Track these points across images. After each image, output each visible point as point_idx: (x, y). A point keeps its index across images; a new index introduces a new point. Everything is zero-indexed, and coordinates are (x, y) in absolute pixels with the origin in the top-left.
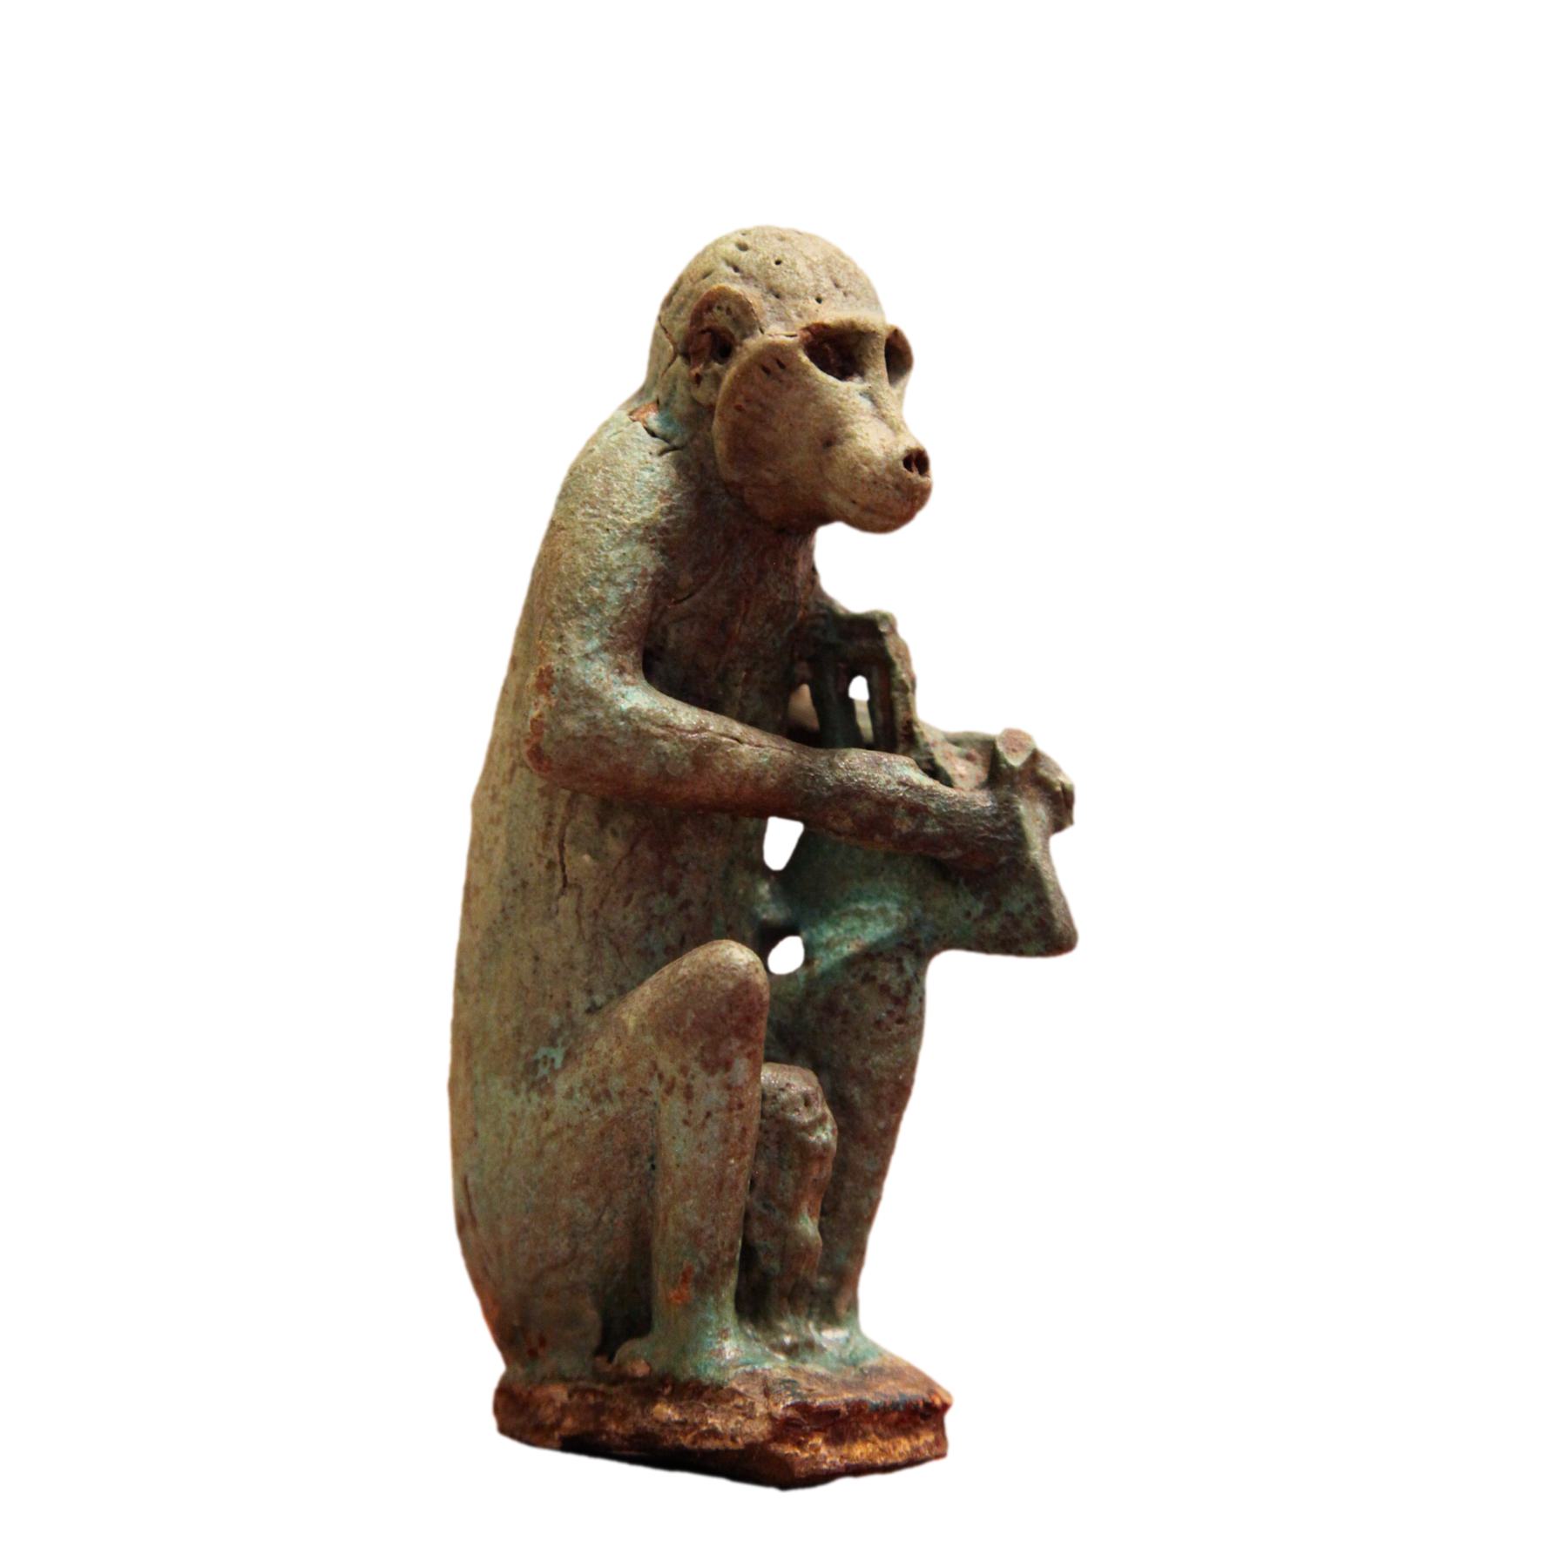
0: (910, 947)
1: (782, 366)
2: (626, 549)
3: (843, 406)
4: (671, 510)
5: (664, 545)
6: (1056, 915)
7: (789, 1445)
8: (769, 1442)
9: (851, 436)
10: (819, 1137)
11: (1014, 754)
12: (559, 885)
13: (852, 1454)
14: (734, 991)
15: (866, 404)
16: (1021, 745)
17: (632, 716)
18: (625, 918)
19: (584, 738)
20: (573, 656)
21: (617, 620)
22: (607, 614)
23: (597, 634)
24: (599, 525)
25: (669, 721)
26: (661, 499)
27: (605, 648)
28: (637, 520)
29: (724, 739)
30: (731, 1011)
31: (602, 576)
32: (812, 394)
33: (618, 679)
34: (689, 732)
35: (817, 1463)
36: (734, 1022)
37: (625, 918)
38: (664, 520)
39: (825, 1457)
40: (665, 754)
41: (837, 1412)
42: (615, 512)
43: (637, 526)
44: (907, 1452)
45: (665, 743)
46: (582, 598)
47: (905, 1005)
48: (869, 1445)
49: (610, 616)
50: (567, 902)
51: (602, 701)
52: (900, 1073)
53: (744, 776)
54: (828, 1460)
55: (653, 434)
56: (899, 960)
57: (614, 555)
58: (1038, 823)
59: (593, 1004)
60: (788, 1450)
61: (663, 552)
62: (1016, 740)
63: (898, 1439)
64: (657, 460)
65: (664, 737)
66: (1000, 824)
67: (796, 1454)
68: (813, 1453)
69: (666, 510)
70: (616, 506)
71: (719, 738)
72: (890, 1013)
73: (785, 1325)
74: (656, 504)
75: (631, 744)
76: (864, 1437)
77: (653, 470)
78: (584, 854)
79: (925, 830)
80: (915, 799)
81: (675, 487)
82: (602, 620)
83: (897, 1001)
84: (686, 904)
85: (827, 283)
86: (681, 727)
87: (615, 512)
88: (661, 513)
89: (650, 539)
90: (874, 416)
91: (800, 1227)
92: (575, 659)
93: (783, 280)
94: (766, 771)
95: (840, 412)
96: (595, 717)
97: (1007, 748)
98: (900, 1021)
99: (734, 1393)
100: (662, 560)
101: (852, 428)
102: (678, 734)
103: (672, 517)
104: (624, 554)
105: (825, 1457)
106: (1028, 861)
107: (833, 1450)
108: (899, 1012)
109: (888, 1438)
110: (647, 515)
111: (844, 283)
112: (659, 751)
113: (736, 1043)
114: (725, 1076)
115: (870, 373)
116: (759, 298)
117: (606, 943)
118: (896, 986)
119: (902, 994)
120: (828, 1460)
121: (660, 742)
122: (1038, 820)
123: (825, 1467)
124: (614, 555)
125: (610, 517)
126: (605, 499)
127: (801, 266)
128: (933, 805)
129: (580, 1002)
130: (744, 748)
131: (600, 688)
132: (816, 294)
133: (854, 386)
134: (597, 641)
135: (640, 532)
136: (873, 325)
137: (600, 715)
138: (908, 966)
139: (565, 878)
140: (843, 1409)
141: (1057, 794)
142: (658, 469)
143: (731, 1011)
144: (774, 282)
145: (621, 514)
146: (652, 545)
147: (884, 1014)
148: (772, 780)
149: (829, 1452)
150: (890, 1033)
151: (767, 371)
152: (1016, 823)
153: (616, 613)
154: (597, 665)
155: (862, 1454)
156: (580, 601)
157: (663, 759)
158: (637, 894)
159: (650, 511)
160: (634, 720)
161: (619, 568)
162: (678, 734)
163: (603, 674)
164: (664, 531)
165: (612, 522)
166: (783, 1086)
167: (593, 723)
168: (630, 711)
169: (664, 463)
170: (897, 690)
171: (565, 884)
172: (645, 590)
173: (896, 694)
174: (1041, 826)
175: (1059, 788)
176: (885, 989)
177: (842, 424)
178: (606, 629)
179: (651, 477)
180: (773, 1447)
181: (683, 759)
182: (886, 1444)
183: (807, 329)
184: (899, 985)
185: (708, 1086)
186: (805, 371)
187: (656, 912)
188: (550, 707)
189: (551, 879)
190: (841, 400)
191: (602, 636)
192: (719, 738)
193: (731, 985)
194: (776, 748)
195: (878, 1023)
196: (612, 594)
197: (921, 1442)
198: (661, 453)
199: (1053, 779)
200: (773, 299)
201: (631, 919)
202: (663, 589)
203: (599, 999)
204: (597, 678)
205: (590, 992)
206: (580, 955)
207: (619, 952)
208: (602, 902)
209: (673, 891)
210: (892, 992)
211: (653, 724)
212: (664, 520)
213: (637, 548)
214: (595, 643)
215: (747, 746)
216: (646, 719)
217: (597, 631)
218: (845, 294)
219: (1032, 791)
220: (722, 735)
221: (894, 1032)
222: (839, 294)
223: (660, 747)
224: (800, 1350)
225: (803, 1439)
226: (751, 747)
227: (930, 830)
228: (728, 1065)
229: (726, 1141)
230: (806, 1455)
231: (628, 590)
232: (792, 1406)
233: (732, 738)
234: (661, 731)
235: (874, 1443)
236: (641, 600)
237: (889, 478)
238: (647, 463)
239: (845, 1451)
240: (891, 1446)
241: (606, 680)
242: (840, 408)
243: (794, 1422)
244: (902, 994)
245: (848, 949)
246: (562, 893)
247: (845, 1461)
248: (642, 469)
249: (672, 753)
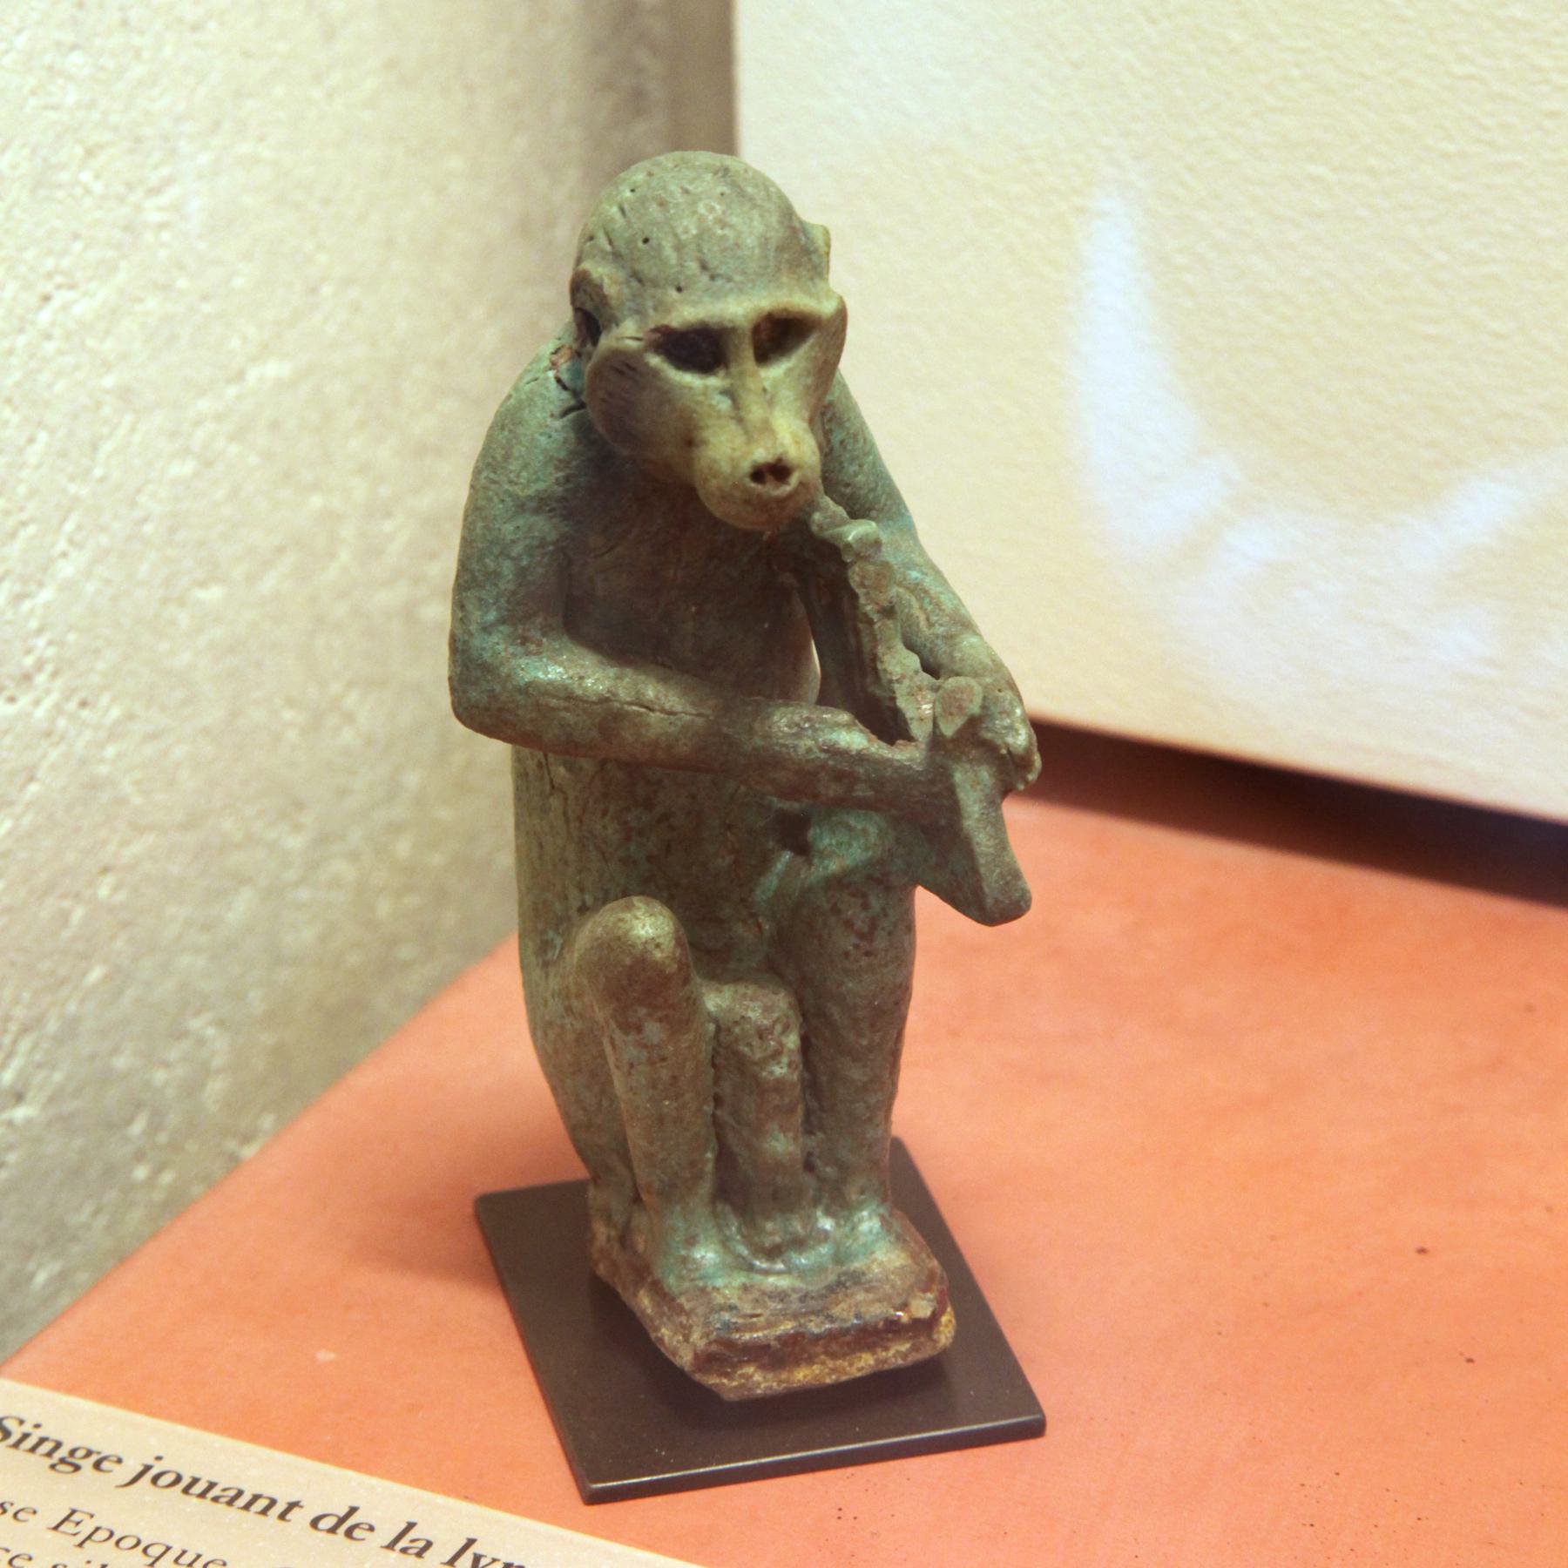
0: (879, 882)
1: (633, 369)
2: (521, 522)
3: (698, 409)
4: (567, 479)
5: (565, 512)
6: (987, 890)
7: (715, 1375)
8: (694, 1372)
9: (705, 442)
10: (771, 1073)
11: (950, 718)
12: (548, 787)
13: (792, 1378)
14: (631, 967)
15: (724, 404)
16: (960, 708)
17: (531, 690)
18: (605, 827)
19: (487, 709)
20: (471, 628)
21: (514, 593)
22: (503, 587)
23: (494, 607)
24: (497, 494)
25: (573, 693)
26: (557, 468)
27: (502, 621)
28: (531, 491)
29: (635, 708)
30: (630, 985)
31: (496, 550)
32: (666, 395)
33: (520, 649)
34: (593, 703)
35: (750, 1389)
36: (635, 995)
37: (605, 827)
38: (561, 489)
39: (759, 1384)
40: (569, 725)
41: (768, 1346)
42: (510, 482)
43: (530, 498)
44: (870, 1365)
45: (568, 714)
46: (479, 570)
47: (872, 941)
48: (815, 1367)
49: (506, 590)
50: (555, 802)
51: (499, 676)
52: (875, 1000)
53: (655, 745)
54: (763, 1386)
55: (565, 388)
56: (865, 896)
57: (509, 528)
58: (979, 787)
59: (584, 902)
60: (712, 1380)
61: (566, 518)
62: (956, 700)
63: (858, 1355)
64: (558, 424)
65: (566, 709)
66: (935, 789)
67: (723, 1384)
68: (743, 1381)
69: (562, 481)
70: (512, 475)
71: (626, 707)
72: (856, 946)
73: (769, 1226)
74: (551, 474)
75: (534, 715)
76: (810, 1360)
77: (550, 437)
78: (560, 765)
79: (855, 794)
80: (839, 767)
81: (573, 454)
82: (498, 593)
83: (861, 936)
84: (666, 817)
85: (693, 266)
86: (585, 699)
87: (510, 482)
88: (557, 482)
89: (547, 508)
90: (732, 418)
91: (767, 1146)
92: (473, 631)
93: (648, 268)
94: (677, 740)
95: (695, 415)
96: (493, 690)
97: (944, 711)
98: (868, 954)
99: (681, 1310)
100: (566, 526)
101: (706, 434)
102: (581, 705)
103: (570, 486)
104: (518, 527)
105: (759, 1384)
106: (961, 829)
107: (770, 1376)
108: (864, 945)
109: (844, 1355)
110: (541, 486)
111: (713, 263)
112: (563, 723)
113: (642, 1011)
114: (637, 1038)
115: (734, 369)
116: (621, 283)
117: (591, 848)
118: (861, 923)
119: (866, 929)
120: (763, 1386)
121: (563, 714)
122: (979, 784)
123: (759, 1391)
124: (509, 528)
125: (506, 487)
126: (504, 465)
127: (669, 252)
128: (861, 770)
129: (575, 903)
130: (654, 717)
131: (497, 662)
132: (676, 283)
133: (715, 381)
134: (495, 613)
135: (533, 504)
136: (731, 321)
137: (498, 688)
138: (876, 903)
139: (551, 781)
140: (773, 1343)
141: (1003, 757)
142: (554, 435)
143: (630, 985)
144: (638, 267)
145: (516, 484)
146: (551, 514)
147: (851, 948)
148: (685, 748)
149: (764, 1378)
150: (858, 964)
151: (621, 372)
152: (951, 790)
153: (511, 587)
154: (495, 638)
155: (805, 1377)
156: (477, 574)
157: (568, 729)
158: (612, 809)
159: (545, 482)
160: (533, 695)
161: (513, 541)
162: (581, 705)
163: (501, 647)
164: (563, 499)
165: (506, 492)
166: (738, 1018)
167: (493, 695)
168: (528, 685)
169: (563, 427)
170: (861, 622)
171: (553, 787)
172: (546, 560)
173: (861, 626)
174: (982, 790)
175: (1004, 751)
176: (849, 924)
177: (697, 428)
178: (503, 601)
179: (548, 443)
180: (698, 1377)
181: (590, 729)
182: (839, 1362)
183: (656, 330)
184: (863, 922)
185: (625, 1042)
186: (655, 373)
187: (634, 824)
188: (456, 673)
189: (542, 778)
190: (697, 403)
191: (498, 609)
192: (626, 707)
193: (628, 961)
194: (691, 714)
195: (847, 954)
196: (507, 568)
197: (891, 1352)
198: (565, 413)
199: (999, 742)
200: (635, 284)
201: (610, 831)
202: (565, 557)
203: (589, 899)
204: (494, 652)
205: (582, 890)
206: (571, 855)
207: (605, 858)
208: (584, 810)
209: (648, 805)
210: (855, 928)
211: (554, 696)
212: (561, 489)
213: (533, 519)
214: (492, 616)
215: (658, 714)
216: (546, 693)
217: (494, 604)
218: (713, 278)
219: (974, 753)
220: (631, 704)
221: (863, 963)
222: (705, 279)
223: (564, 718)
224: (784, 1249)
225: (729, 1370)
226: (662, 716)
227: (860, 794)
228: (639, 1029)
229: (654, 1087)
230: (735, 1383)
231: (524, 563)
232: (715, 1341)
233: (642, 706)
234: (562, 704)
235: (823, 1363)
236: (540, 570)
237: (737, 494)
238: (547, 426)
239: (784, 1376)
240: (846, 1364)
241: (503, 654)
242: (695, 412)
243: (717, 1356)
244: (866, 929)
245: (834, 866)
246: (551, 794)
247: (784, 1385)
248: (541, 434)
249: (576, 724)
